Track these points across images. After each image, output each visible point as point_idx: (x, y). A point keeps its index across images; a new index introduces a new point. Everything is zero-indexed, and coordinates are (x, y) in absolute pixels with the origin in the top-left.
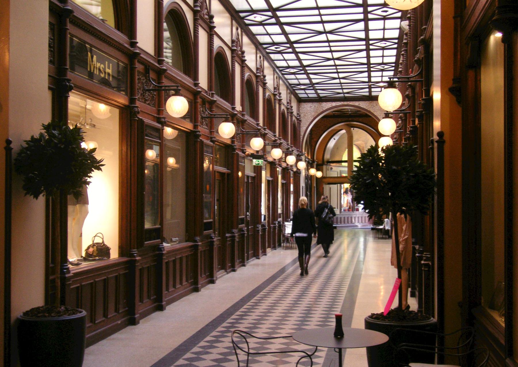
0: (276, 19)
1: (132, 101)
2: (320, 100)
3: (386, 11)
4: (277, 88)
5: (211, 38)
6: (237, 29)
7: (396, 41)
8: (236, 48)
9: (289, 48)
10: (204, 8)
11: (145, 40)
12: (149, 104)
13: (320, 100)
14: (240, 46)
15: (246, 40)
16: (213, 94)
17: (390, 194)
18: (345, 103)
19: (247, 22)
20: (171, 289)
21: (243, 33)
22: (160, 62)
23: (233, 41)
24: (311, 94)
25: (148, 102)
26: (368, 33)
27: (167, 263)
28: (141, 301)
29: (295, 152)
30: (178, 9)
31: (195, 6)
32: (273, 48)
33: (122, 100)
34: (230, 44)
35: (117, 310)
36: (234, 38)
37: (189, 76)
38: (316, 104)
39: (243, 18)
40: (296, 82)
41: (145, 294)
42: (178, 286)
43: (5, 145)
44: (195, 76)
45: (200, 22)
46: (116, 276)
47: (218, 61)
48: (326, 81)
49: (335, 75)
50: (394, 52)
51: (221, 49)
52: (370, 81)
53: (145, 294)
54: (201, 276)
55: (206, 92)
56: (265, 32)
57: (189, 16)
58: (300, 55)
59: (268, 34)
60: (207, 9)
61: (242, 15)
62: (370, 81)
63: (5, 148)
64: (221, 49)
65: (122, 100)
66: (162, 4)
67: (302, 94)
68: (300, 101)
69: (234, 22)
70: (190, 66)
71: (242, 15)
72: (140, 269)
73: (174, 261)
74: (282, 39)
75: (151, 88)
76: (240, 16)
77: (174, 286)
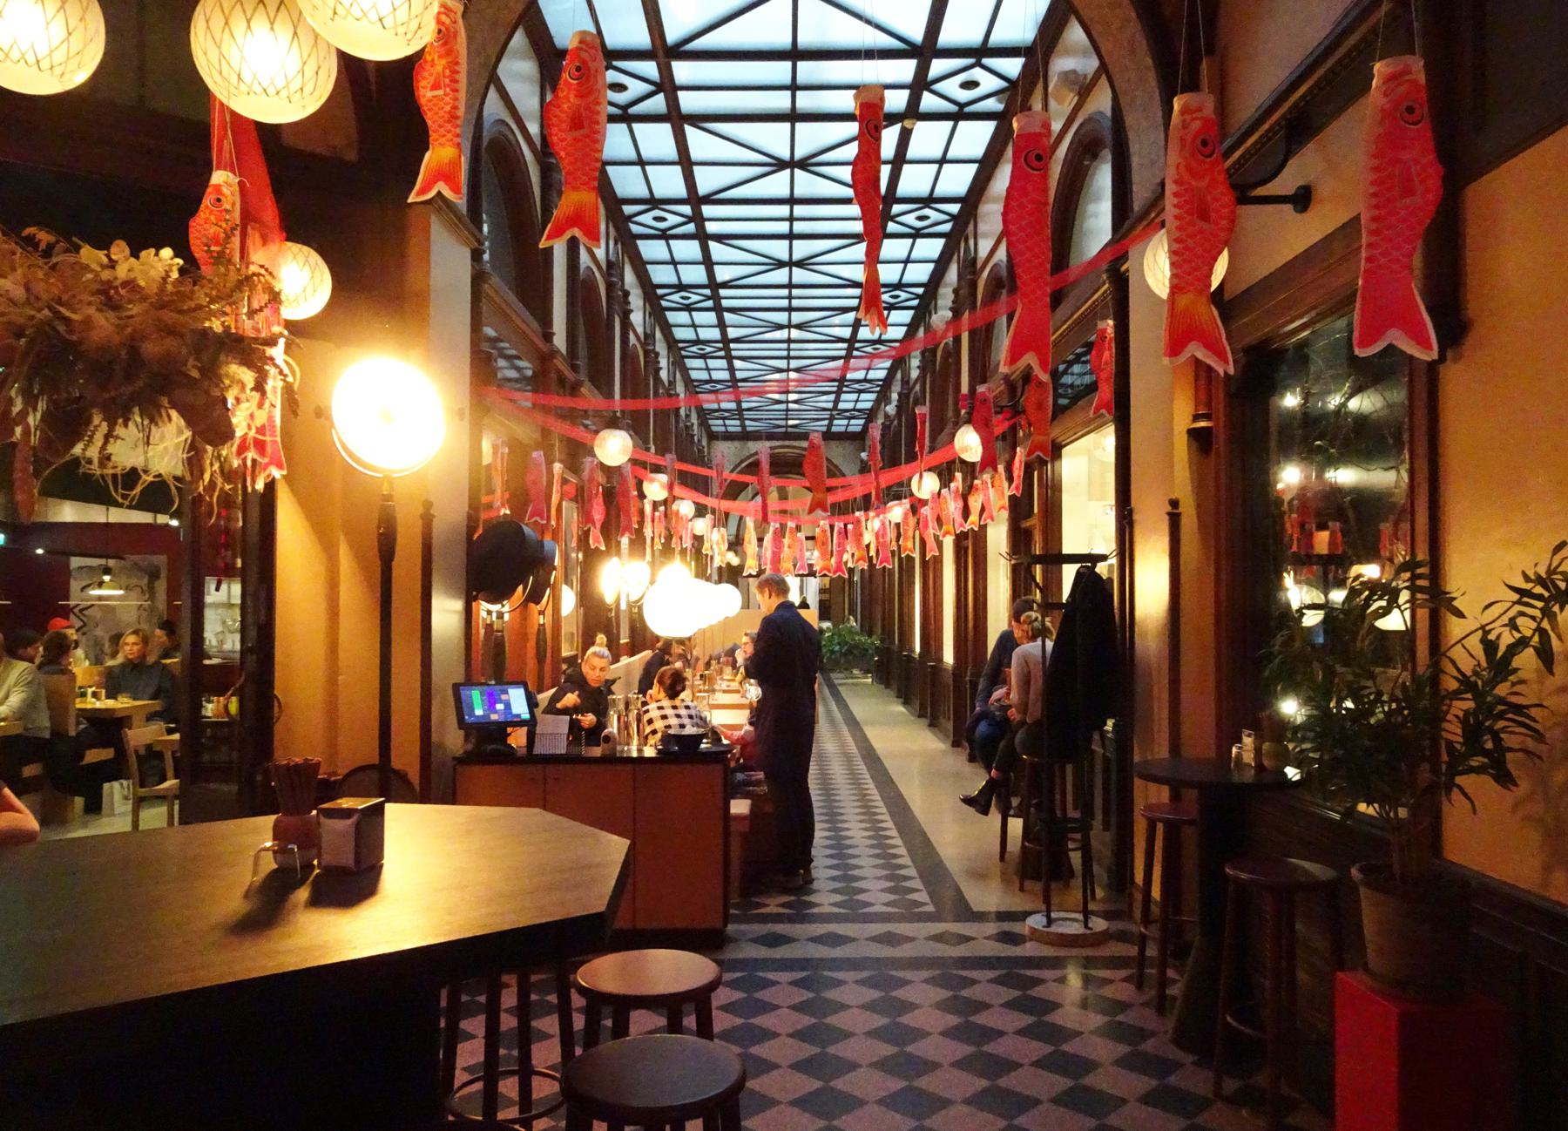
2: (745, 436)
3: (920, 218)
4: (649, 337)
7: (920, 291)
9: (708, 298)
13: (745, 436)
17: (40, 551)
18: (787, 443)
19: (635, 229)
24: (734, 425)
26: (900, 170)
32: (694, 349)
34: (604, 266)
36: (612, 258)
38: (737, 444)
39: (630, 218)
40: (704, 375)
48: (761, 410)
49: (782, 318)
50: (873, 396)
51: (503, 129)
52: (835, 407)
58: (727, 315)
59: (673, 262)
61: (660, 292)
62: (835, 407)
64: (503, 129)
67: (717, 425)
68: (713, 436)
74: (696, 275)
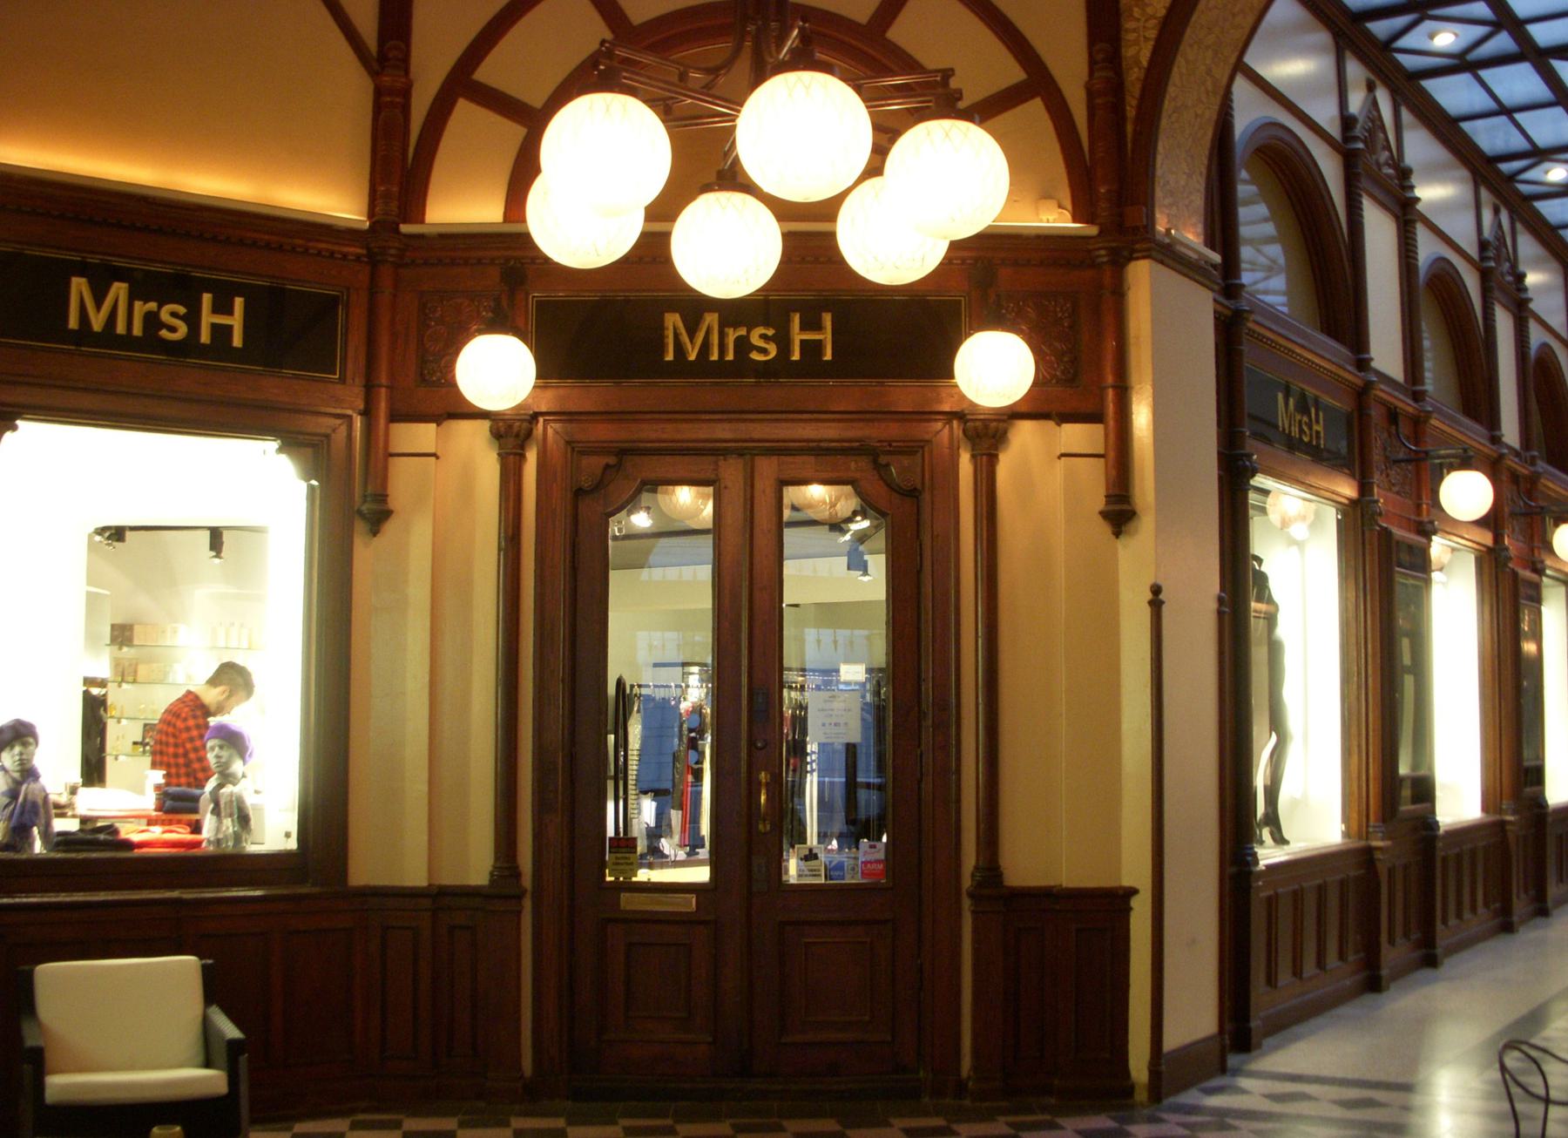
0: (1512, 34)
1: (1364, 488)
5: (1406, 231)
6: (1496, 211)
8: (1495, 264)
10: (1379, 147)
11: (1386, 353)
12: (1398, 493)
14: (1508, 260)
15: (1527, 246)
16: (1533, 458)
20: (1452, 921)
21: (1519, 226)
22: (1418, 396)
23: (1483, 245)
25: (1395, 489)
27: (1444, 859)
28: (1391, 941)
29: (1511, 462)
30: (1281, 140)
31: (1483, 259)
33: (1348, 490)
34: (1473, 251)
35: (1342, 956)
37: (1476, 419)
39: (1512, 177)
41: (1399, 930)
42: (1467, 915)
43: (1149, 596)
44: (1491, 420)
45: (1497, 294)
46: (1295, 893)
47: (1431, 293)
53: (1399, 930)
54: (1391, 941)
55: (1517, 454)
56: (1491, 105)
57: (1471, 281)
60: (1388, 147)
61: (1506, 167)
63: (1151, 603)
65: (1348, 490)
66: (1416, 266)
69: (1485, 194)
70: (1477, 399)
71: (1506, 167)
72: (1269, 899)
73: (1459, 857)
75: (1401, 456)
76: (1499, 172)
77: (1459, 915)
